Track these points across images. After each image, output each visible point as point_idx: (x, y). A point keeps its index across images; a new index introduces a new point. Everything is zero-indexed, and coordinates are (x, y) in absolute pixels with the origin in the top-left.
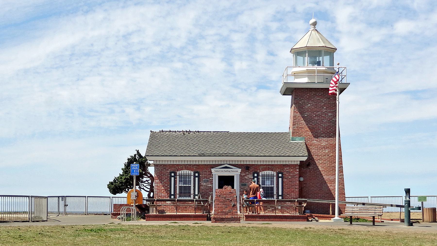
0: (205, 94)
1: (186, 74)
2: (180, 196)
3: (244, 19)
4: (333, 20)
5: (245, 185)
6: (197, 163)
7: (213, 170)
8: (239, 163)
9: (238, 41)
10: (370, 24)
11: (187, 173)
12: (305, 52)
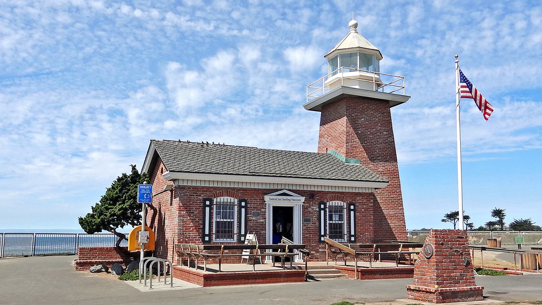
0: (34, 157)
1: (21, 143)
2: (217, 237)
3: (67, 110)
4: (126, 116)
5: (309, 220)
6: (244, 186)
7: (267, 198)
8: (302, 189)
9: (61, 124)
10: (150, 121)
11: (229, 201)
12: (355, 54)
